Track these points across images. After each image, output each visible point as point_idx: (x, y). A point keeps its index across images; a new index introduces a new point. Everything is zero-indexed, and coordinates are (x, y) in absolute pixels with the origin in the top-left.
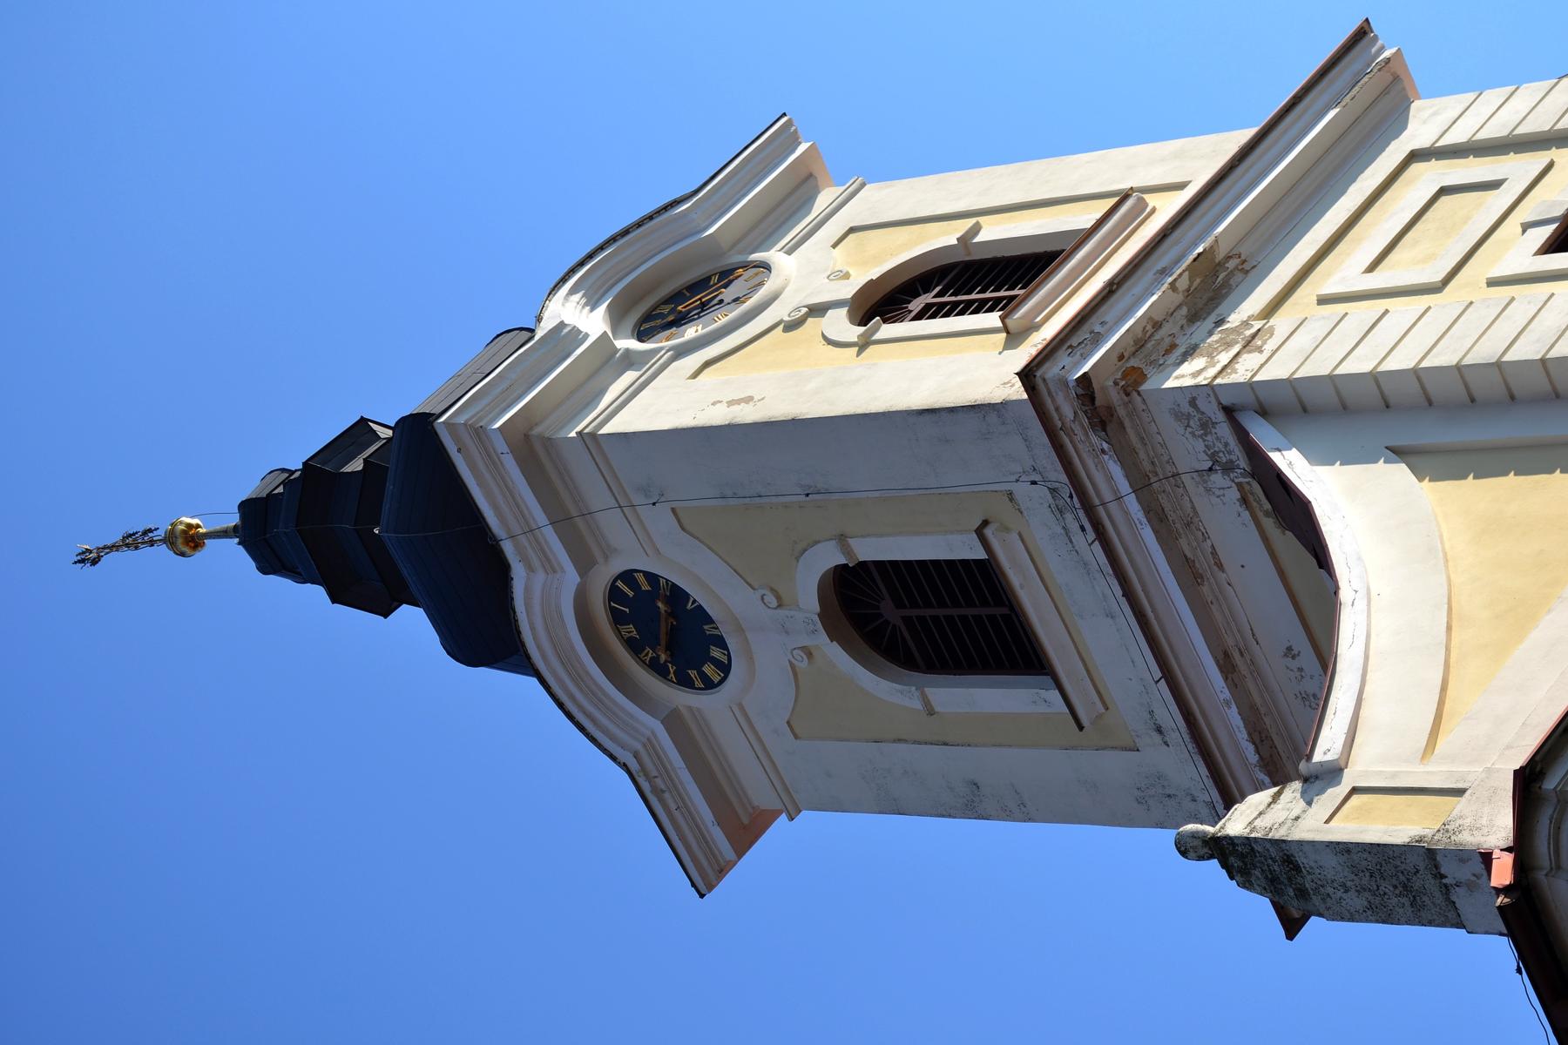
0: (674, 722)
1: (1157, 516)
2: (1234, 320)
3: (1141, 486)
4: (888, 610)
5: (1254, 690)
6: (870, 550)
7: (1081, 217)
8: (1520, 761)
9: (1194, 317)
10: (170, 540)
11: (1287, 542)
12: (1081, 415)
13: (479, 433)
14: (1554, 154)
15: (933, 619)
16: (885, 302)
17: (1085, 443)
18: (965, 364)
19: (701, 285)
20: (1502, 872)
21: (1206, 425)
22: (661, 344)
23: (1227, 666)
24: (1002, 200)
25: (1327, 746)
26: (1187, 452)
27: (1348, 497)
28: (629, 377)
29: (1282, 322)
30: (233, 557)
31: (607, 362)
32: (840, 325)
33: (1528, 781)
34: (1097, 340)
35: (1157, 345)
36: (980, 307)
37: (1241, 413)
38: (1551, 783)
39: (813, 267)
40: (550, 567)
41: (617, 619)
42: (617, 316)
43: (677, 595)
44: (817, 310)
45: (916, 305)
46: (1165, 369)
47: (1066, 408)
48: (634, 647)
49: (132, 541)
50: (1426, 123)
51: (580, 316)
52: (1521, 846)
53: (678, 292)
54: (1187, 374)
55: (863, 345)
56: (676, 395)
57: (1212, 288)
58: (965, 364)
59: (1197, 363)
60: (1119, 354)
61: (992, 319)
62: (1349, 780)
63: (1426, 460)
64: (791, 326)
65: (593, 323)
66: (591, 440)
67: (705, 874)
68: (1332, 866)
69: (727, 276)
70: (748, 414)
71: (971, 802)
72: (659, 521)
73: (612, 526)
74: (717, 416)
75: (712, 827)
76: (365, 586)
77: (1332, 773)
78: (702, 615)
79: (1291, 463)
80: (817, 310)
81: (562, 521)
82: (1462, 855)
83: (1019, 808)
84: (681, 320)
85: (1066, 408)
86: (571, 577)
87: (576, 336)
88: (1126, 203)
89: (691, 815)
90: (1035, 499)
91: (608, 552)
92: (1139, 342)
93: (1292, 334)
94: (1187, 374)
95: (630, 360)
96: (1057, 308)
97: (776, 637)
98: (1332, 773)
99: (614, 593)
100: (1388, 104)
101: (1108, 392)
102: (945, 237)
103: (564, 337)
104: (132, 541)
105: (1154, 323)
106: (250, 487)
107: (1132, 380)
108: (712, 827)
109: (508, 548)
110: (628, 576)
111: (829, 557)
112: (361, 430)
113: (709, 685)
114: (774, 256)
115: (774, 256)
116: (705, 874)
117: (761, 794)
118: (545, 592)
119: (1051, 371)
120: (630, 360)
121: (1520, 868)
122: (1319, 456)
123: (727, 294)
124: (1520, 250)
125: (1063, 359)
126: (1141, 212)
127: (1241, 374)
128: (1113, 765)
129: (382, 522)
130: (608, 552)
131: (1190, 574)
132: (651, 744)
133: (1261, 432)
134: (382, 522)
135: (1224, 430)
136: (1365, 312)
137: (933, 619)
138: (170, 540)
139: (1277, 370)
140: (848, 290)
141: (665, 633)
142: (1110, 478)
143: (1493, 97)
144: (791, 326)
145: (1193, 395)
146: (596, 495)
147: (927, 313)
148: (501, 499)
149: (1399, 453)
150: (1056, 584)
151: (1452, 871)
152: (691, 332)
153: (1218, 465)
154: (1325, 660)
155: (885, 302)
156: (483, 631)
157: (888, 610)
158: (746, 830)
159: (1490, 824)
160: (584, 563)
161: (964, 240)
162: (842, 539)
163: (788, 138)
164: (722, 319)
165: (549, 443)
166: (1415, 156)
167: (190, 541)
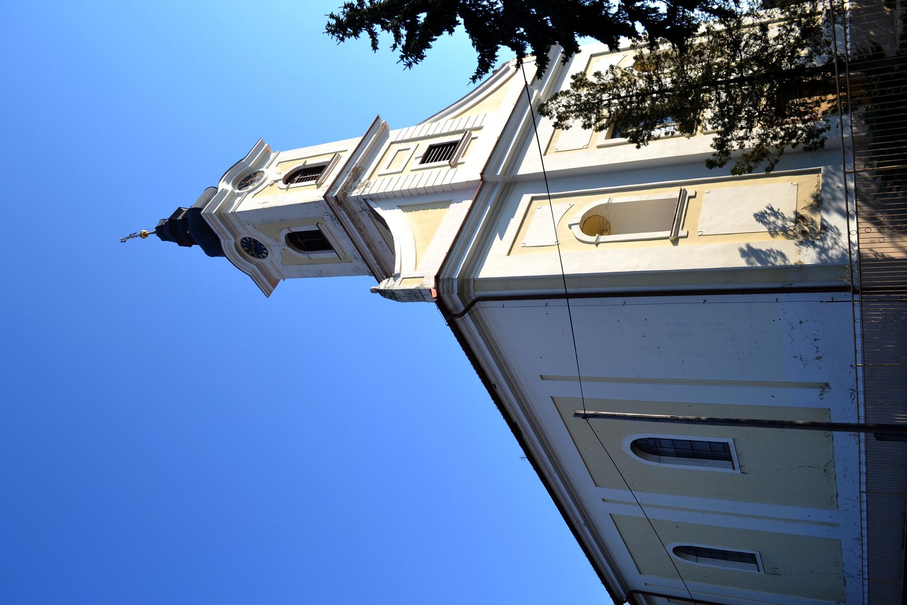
0: (257, 265)
1: (353, 220)
2: (363, 180)
3: (349, 215)
4: (299, 240)
5: (378, 260)
6: (294, 230)
7: (327, 158)
8: (435, 274)
9: (355, 181)
10: (140, 235)
11: (378, 223)
12: (336, 203)
13: (210, 214)
14: (419, 142)
15: (308, 241)
16: (290, 179)
17: (337, 208)
18: (309, 193)
19: (250, 177)
20: (434, 294)
21: (360, 203)
22: (244, 191)
23: (369, 246)
24: (311, 155)
25: (397, 271)
26: (357, 208)
27: (392, 217)
28: (239, 199)
29: (372, 180)
30: (155, 238)
31: (234, 196)
32: (281, 184)
33: (437, 278)
34: (337, 188)
35: (348, 188)
36: (309, 179)
37: (367, 200)
38: (441, 277)
39: (274, 171)
40: (228, 239)
41: (243, 247)
42: (233, 185)
43: (255, 241)
44: (276, 181)
45: (296, 179)
46: (351, 192)
47: (333, 202)
48: (247, 251)
49: (131, 236)
50: (393, 135)
51: (225, 186)
52: (437, 287)
53: (246, 179)
54: (355, 193)
55: (287, 189)
56: (250, 202)
57: (357, 174)
58: (309, 193)
59: (357, 191)
60: (342, 190)
61: (313, 182)
62: (402, 276)
63: (406, 208)
64: (271, 185)
65: (229, 187)
66: (234, 213)
67: (268, 293)
68: (401, 293)
69: (255, 174)
70: (266, 206)
71: (320, 274)
72: (250, 228)
73: (240, 229)
74: (260, 207)
75: (268, 284)
76: (185, 242)
77: (398, 275)
78: (261, 244)
79: (378, 210)
80: (276, 181)
81: (230, 229)
82: (425, 290)
83: (330, 274)
84: (247, 185)
85: (333, 202)
86: (233, 240)
87: (226, 191)
88: (336, 156)
89: (264, 283)
90: (328, 220)
91: (240, 234)
92: (345, 187)
93: (375, 183)
94: (355, 193)
95: (238, 195)
96: (329, 179)
97: (277, 249)
98: (398, 275)
99: (242, 242)
100: (384, 134)
101: (341, 198)
102: (299, 164)
103: (224, 192)
104: (131, 236)
105: (347, 183)
106: (157, 224)
107: (345, 195)
108: (268, 284)
109: (219, 236)
110: (244, 238)
111: (286, 232)
112: (179, 210)
113: (264, 257)
114: (263, 169)
115: (263, 169)
116: (268, 293)
117: (276, 276)
118: (228, 242)
119: (329, 195)
120: (238, 195)
121: (438, 293)
122: (384, 208)
123: (256, 178)
124: (415, 163)
125: (331, 192)
126: (339, 157)
127: (366, 193)
128: (347, 265)
129: (188, 228)
130: (240, 234)
131: (360, 230)
132: (253, 270)
133: (372, 204)
134: (188, 228)
135: (364, 203)
136: (388, 178)
137: (308, 241)
138: (140, 235)
139: (373, 192)
140: (282, 177)
141: (253, 249)
142: (343, 214)
143: (405, 129)
144: (271, 185)
145: (357, 197)
146: (236, 224)
147: (299, 181)
148: (216, 227)
149: (399, 207)
150: (333, 233)
151: (424, 293)
152: (250, 187)
153: (363, 210)
154: (393, 253)
155: (290, 179)
156: (213, 248)
157: (299, 240)
158: (274, 284)
159: (430, 284)
160: (235, 237)
161: (304, 164)
162: (289, 228)
163: (262, 144)
164: (256, 184)
165: (225, 214)
166: (392, 143)
167: (145, 235)
